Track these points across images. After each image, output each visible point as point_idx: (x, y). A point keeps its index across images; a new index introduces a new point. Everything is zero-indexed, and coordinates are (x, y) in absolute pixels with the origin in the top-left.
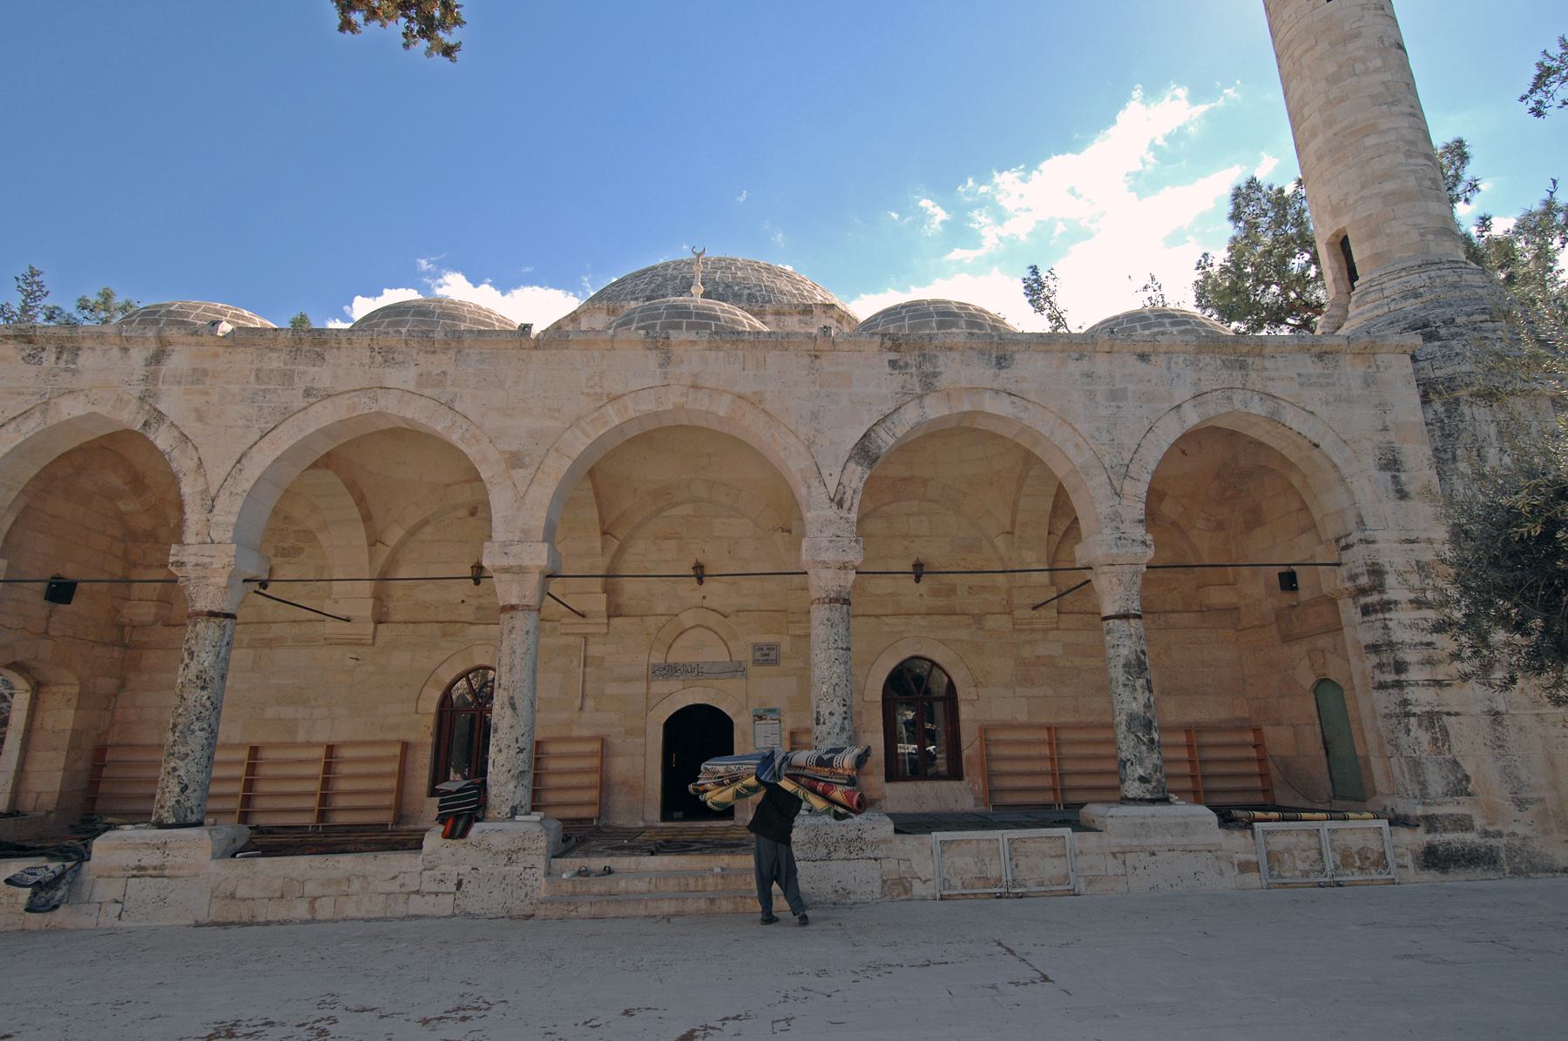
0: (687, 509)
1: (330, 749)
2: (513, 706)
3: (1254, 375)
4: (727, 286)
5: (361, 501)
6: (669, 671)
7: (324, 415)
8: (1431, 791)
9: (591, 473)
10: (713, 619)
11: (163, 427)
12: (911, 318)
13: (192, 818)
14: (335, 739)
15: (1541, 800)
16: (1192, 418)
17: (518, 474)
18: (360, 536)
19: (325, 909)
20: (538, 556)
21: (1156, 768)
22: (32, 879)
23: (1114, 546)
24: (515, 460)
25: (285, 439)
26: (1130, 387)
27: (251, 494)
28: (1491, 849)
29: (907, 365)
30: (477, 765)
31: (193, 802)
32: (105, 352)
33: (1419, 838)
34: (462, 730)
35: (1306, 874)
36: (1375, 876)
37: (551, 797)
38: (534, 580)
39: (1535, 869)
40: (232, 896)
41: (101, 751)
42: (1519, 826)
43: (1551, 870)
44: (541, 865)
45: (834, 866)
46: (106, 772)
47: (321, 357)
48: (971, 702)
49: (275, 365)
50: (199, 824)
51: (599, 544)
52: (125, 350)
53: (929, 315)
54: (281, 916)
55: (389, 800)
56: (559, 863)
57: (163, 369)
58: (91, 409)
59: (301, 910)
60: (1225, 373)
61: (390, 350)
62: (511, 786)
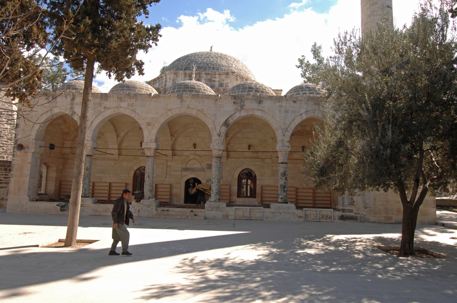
1: (110, 183)
2: (149, 177)
3: (321, 107)
4: (207, 64)
5: (114, 127)
6: (187, 169)
7: (108, 113)
8: (345, 204)
9: (168, 123)
10: (197, 157)
11: (75, 115)
12: (242, 89)
13: (87, 196)
14: (111, 181)
15: (370, 207)
16: (304, 117)
17: (149, 127)
18: (114, 135)
20: (153, 146)
21: (285, 196)
23: (282, 145)
24: (149, 124)
25: (100, 118)
26: (290, 109)
28: (356, 217)
29: (237, 103)
30: (142, 187)
31: (87, 193)
32: (62, 98)
33: (341, 213)
34: (139, 178)
35: (313, 219)
36: (328, 220)
37: (159, 197)
38: (153, 150)
40: (96, 211)
43: (369, 222)
45: (213, 212)
46: (62, 186)
47: (107, 99)
50: (88, 197)
51: (170, 138)
52: (66, 97)
54: (106, 215)
57: (74, 102)
58: (61, 111)
60: (314, 106)
61: (121, 98)
62: (149, 193)
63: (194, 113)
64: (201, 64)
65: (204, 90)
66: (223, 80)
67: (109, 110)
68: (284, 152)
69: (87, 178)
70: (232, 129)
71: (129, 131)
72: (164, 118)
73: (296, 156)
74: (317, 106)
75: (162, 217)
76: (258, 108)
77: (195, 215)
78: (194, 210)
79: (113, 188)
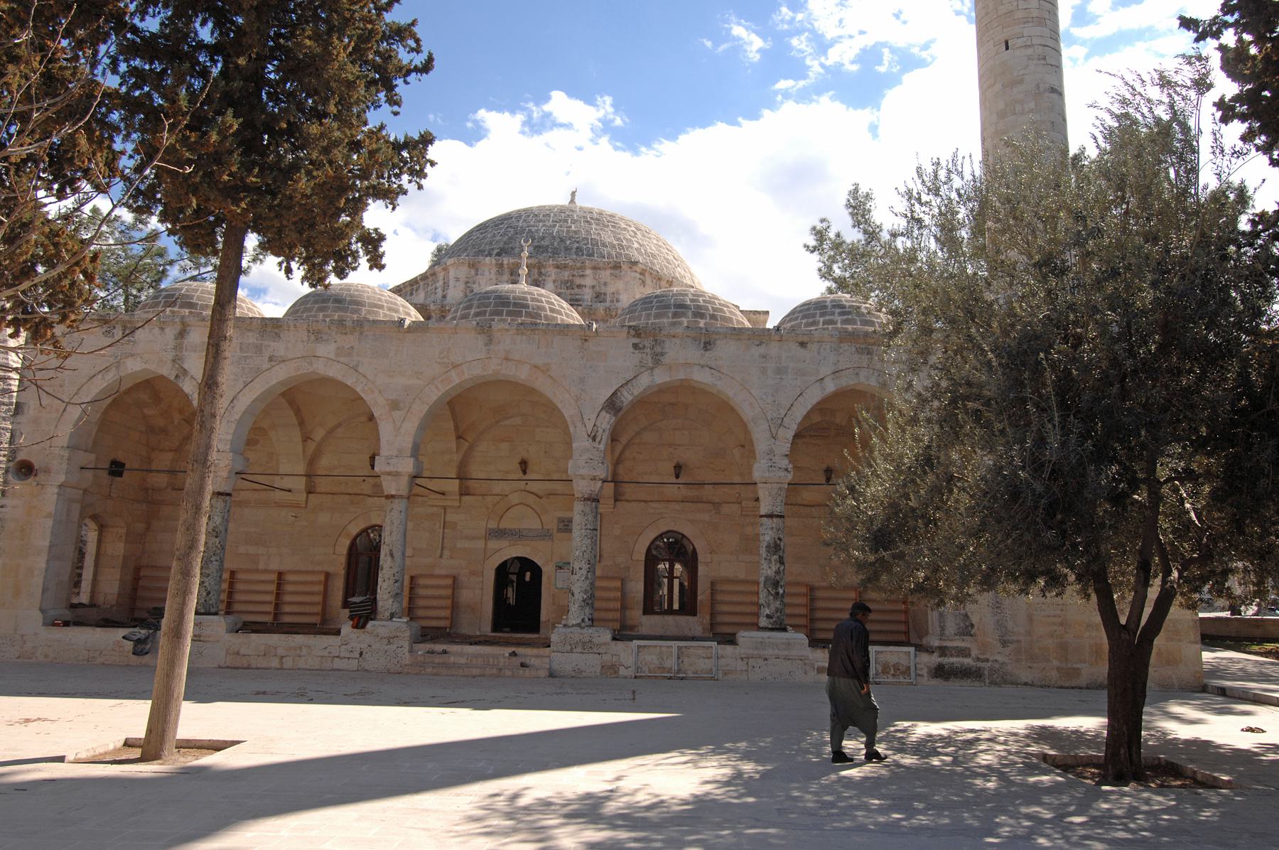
0: (517, 421)
1: (280, 574)
2: (392, 555)
4: (562, 240)
5: (298, 412)
6: (500, 533)
8: (947, 632)
9: (450, 403)
10: (531, 500)
12: (658, 308)
13: (213, 610)
14: (283, 568)
15: (1018, 641)
16: (830, 387)
17: (397, 414)
18: (297, 435)
19: (288, 663)
20: (407, 466)
22: (135, 638)
24: (394, 405)
27: (239, 422)
28: (979, 669)
33: (935, 659)
34: (363, 560)
36: (902, 680)
37: (420, 613)
38: (404, 481)
39: (1005, 682)
40: (238, 653)
41: (138, 569)
42: (1000, 656)
43: (1015, 683)
44: (406, 645)
48: (707, 564)
49: (251, 340)
50: (216, 614)
51: (454, 445)
52: (162, 329)
53: (668, 307)
55: (318, 609)
56: (417, 646)
59: (275, 663)
61: (319, 332)
63: (522, 374)
64: (543, 238)
65: (552, 310)
66: (605, 284)
67: (282, 365)
68: (775, 486)
69: (213, 558)
70: (630, 419)
71: (339, 425)
72: (437, 388)
73: (808, 495)
74: (865, 358)
75: (429, 670)
76: (702, 362)
77: (523, 665)
78: (520, 650)
79: (289, 588)
